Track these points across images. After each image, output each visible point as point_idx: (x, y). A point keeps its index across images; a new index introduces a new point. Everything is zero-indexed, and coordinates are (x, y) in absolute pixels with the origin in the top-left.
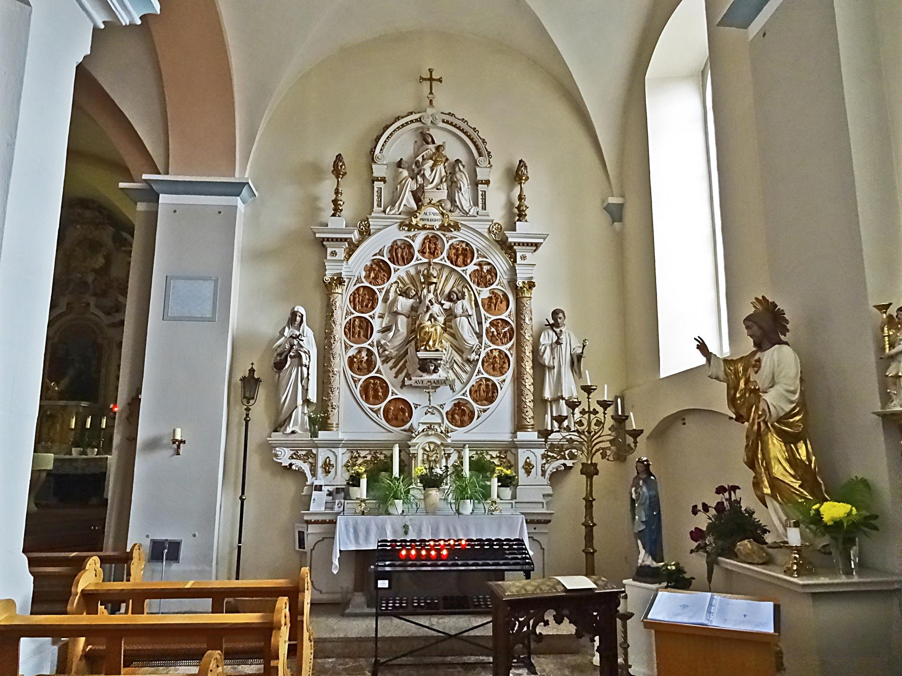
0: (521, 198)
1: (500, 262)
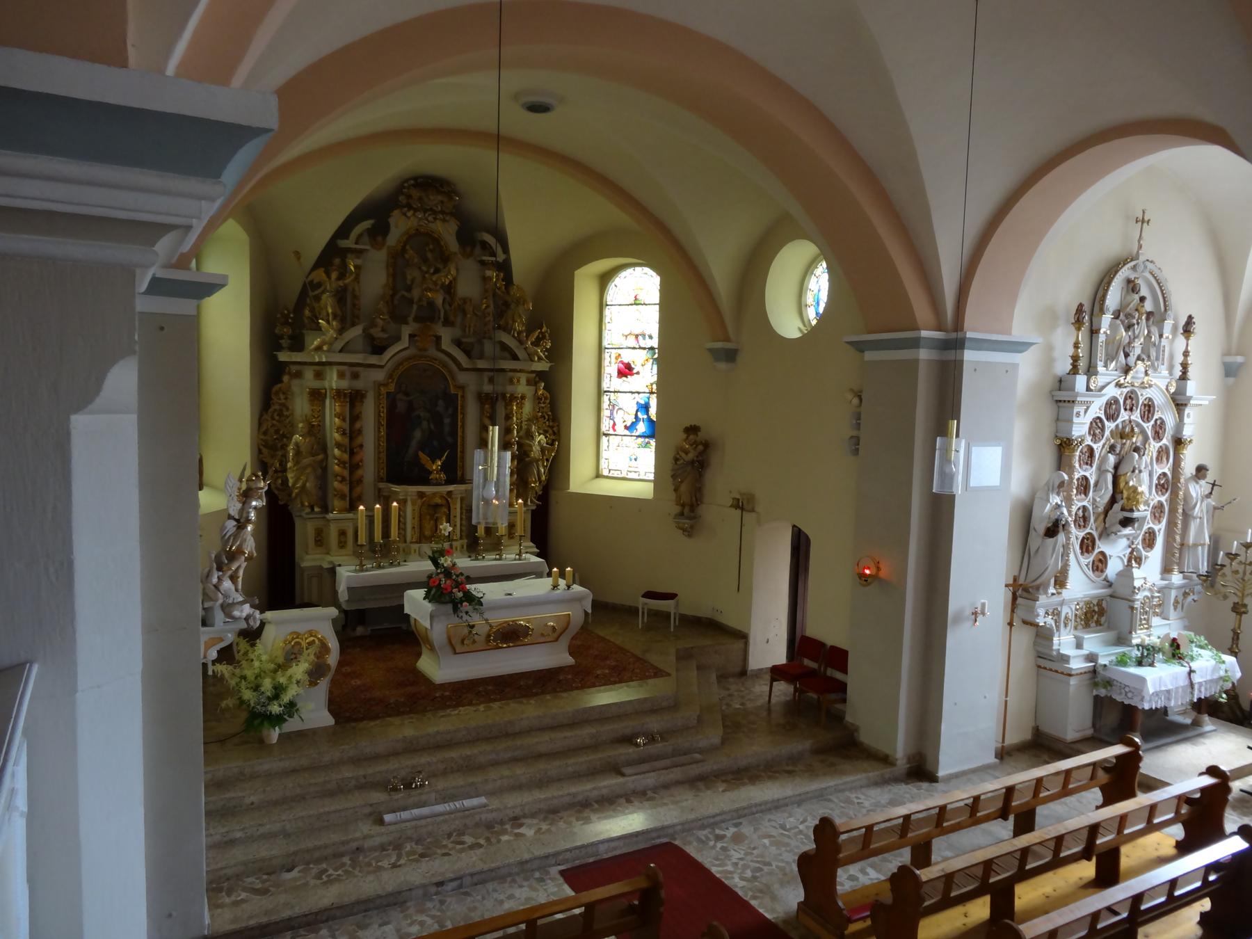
0: (1186, 354)
1: (1170, 419)
